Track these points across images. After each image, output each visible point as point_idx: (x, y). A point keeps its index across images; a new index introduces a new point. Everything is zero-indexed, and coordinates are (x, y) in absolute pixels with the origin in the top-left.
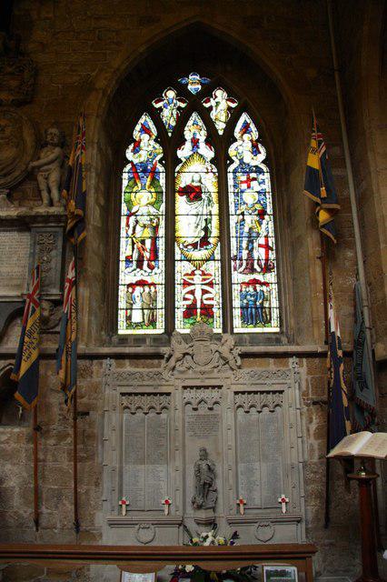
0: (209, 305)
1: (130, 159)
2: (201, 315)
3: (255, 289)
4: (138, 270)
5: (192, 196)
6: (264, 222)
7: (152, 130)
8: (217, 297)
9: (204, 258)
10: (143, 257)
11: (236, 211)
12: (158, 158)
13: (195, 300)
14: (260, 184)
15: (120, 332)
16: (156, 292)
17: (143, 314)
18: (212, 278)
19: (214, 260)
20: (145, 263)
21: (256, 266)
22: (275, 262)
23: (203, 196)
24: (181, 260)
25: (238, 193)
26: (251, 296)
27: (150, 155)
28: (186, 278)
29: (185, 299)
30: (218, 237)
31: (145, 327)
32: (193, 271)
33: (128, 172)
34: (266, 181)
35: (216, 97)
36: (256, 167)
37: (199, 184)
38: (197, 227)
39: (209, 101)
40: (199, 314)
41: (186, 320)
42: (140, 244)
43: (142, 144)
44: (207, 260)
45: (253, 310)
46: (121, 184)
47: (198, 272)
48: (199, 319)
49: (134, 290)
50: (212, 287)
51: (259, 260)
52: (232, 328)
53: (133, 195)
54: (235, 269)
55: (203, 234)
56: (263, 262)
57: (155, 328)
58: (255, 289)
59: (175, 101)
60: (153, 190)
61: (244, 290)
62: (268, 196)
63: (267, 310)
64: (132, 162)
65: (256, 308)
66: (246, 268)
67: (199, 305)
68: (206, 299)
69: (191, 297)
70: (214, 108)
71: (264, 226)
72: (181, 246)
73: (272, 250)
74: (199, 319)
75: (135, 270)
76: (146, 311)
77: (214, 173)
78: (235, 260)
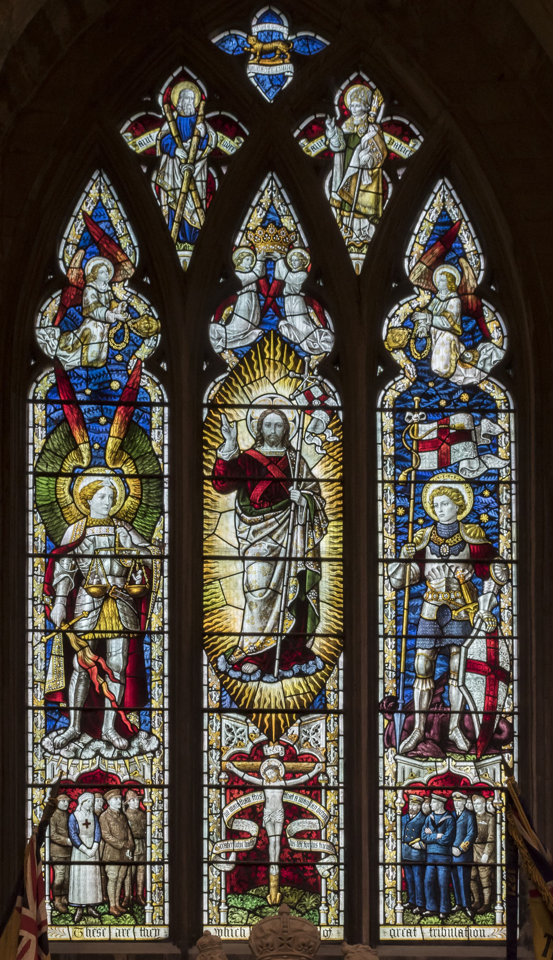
0: (306, 854)
1: (49, 352)
2: (282, 882)
3: (449, 807)
4: (87, 739)
5: (258, 491)
6: (489, 586)
7: (124, 243)
8: (332, 829)
9: (293, 702)
10: (102, 697)
11: (398, 546)
12: (143, 352)
13: (263, 836)
14: (481, 452)
15: (385, 934)
16: (142, 810)
17: (105, 880)
18: (319, 767)
19: (327, 712)
20: (110, 717)
21: (456, 735)
22: (515, 721)
23: (295, 494)
24: (221, 711)
25: (407, 483)
26: (436, 827)
27: (118, 338)
28: (234, 768)
29: (233, 835)
30: (338, 635)
31: (109, 919)
32: (258, 748)
33: (47, 401)
34: (503, 440)
35: (346, 114)
36: (472, 389)
37: (279, 451)
38: (270, 601)
39: (322, 130)
40: (273, 883)
41: (234, 901)
42: (90, 655)
43: (90, 296)
44: (302, 712)
45: (441, 871)
46: (23, 443)
47: (270, 750)
48: (274, 896)
49: (74, 803)
50: (317, 799)
51: (465, 712)
52: (375, 927)
53: (64, 482)
54: (390, 742)
55: (290, 625)
56: (477, 721)
57: (140, 922)
58: (449, 807)
59: (200, 127)
60: (128, 469)
61: (413, 807)
62: (504, 497)
63: (484, 873)
64: (56, 362)
65: (451, 867)
66: (423, 740)
67: (274, 853)
68: (299, 835)
69: (251, 828)
70: (337, 159)
71: (484, 602)
72: (222, 666)
73: (508, 681)
74: (274, 896)
75: (74, 739)
76: (112, 871)
77: (331, 411)
78: (392, 711)
